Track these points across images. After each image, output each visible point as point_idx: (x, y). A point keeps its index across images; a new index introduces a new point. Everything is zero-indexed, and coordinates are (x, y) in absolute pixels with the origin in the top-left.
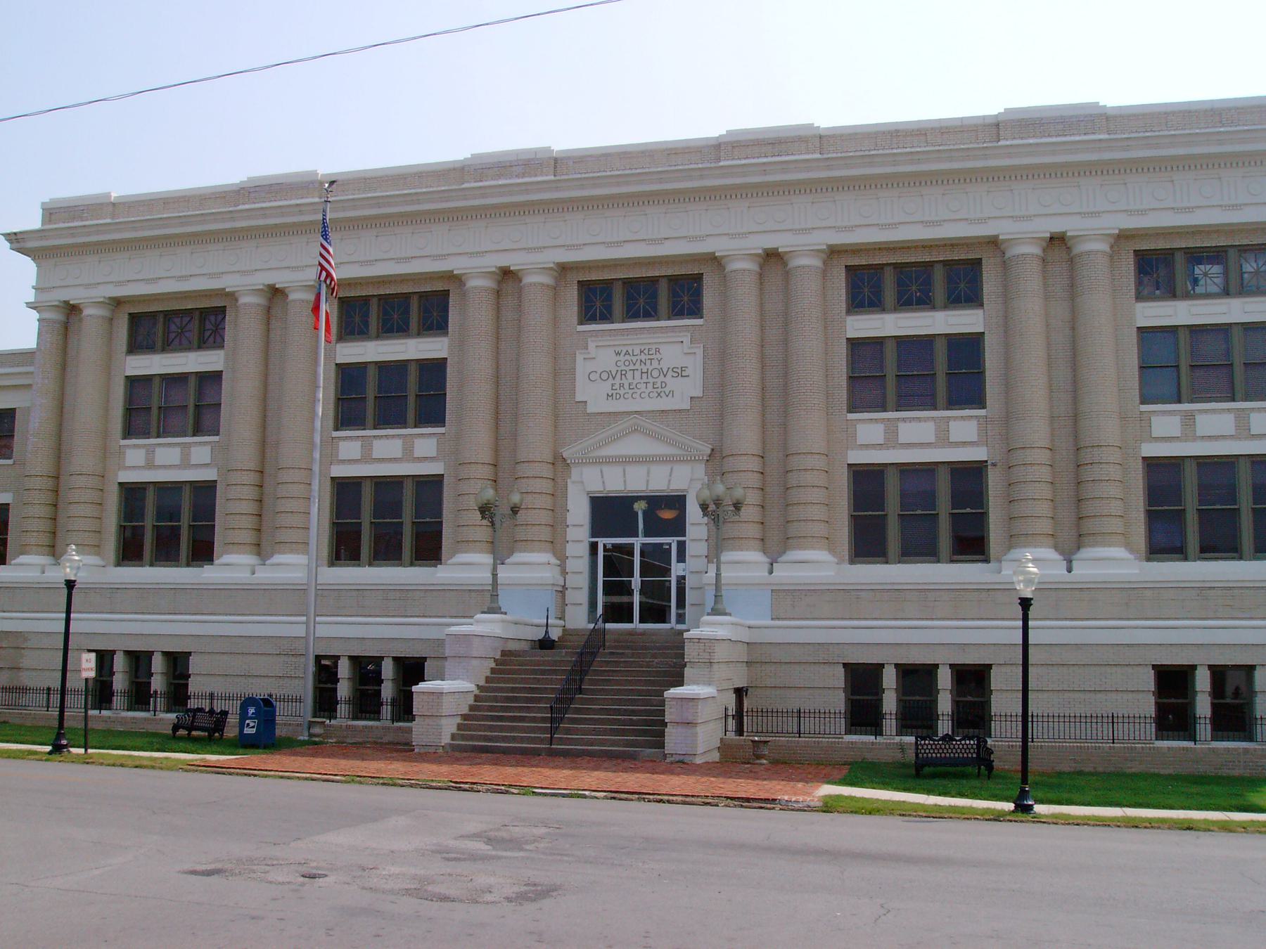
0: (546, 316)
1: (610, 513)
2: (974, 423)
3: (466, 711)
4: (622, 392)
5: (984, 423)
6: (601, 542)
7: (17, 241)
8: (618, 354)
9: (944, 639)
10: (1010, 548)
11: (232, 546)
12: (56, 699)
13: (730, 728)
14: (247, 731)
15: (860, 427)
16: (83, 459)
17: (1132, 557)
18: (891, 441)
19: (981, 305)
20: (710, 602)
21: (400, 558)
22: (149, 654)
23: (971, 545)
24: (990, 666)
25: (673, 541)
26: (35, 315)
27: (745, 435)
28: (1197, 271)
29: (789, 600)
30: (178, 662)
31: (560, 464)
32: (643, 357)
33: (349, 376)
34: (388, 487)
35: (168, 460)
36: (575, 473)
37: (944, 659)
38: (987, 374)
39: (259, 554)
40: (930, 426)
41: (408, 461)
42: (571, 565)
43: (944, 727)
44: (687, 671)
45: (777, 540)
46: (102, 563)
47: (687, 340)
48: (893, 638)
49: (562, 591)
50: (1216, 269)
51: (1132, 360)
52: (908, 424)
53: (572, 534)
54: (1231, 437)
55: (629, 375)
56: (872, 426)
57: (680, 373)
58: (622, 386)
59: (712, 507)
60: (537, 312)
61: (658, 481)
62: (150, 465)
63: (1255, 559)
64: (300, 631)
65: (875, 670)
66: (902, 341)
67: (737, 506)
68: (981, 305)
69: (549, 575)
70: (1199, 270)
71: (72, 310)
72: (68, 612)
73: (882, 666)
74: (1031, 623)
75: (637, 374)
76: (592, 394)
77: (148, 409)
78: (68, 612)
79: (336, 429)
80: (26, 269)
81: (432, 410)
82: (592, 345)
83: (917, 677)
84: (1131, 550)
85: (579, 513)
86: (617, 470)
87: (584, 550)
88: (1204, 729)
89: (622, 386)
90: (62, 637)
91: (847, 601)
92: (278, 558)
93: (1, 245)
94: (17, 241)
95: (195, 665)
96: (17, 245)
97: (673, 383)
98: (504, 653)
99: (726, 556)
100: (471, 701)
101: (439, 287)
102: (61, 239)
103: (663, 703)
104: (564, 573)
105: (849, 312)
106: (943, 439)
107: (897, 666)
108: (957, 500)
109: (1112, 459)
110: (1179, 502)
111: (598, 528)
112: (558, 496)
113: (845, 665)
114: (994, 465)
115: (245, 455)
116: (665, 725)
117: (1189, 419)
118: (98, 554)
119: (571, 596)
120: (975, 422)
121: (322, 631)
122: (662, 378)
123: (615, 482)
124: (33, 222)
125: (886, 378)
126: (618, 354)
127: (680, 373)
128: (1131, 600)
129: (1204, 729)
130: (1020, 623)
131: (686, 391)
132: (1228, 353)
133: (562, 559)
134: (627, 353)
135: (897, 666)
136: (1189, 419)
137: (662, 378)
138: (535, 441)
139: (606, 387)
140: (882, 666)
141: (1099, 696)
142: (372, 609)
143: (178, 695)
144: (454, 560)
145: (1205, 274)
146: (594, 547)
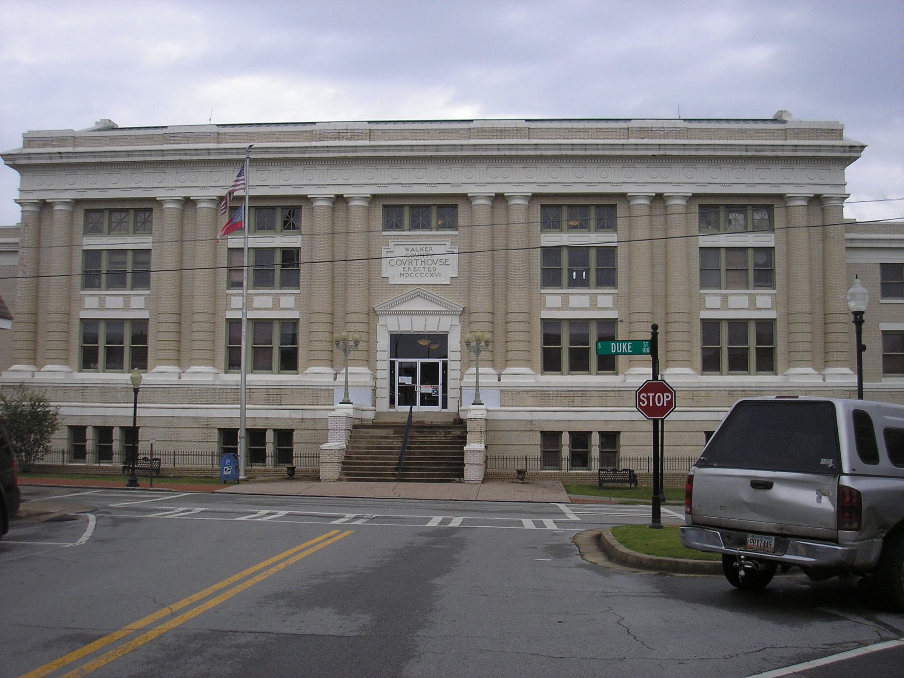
1: (401, 343)
2: (611, 297)
4: (409, 272)
5: (147, 298)
6: (398, 361)
7: (11, 160)
8: (407, 250)
10: (789, 367)
11: (312, 362)
13: (215, 462)
14: (225, 473)
15: (548, 297)
16: (54, 302)
17: (692, 372)
18: (565, 306)
19: (616, 231)
23: (290, 362)
24: (619, 432)
25: (440, 361)
26: (19, 208)
27: (481, 301)
28: (731, 217)
29: (509, 395)
30: (285, 436)
31: (372, 313)
33: (551, 254)
34: (738, 326)
35: (272, 304)
36: (381, 320)
37: (595, 428)
38: (619, 270)
39: (35, 364)
40: (587, 298)
42: (379, 374)
45: (501, 362)
46: (71, 370)
47: (448, 244)
48: (564, 417)
49: (374, 390)
50: (741, 216)
52: (574, 297)
53: (380, 356)
54: (123, 309)
55: (414, 262)
58: (409, 269)
59: (473, 344)
60: (357, 220)
61: (432, 325)
62: (102, 308)
63: (756, 374)
64: (237, 414)
65: (557, 435)
66: (571, 248)
67: (357, 343)
68: (616, 231)
69: (368, 380)
70: (732, 216)
71: (44, 205)
73: (113, 427)
75: (419, 262)
76: (392, 272)
77: (96, 271)
79: (228, 289)
80: (14, 176)
81: (142, 278)
82: (391, 244)
83: (580, 439)
84: (694, 369)
85: (384, 343)
86: (408, 318)
87: (386, 365)
88: (565, 464)
89: (409, 269)
90: (132, 419)
91: (543, 396)
92: (48, 367)
93: (864, 143)
94: (11, 160)
96: (11, 163)
97: (440, 269)
98: (355, 427)
100: (344, 454)
101: (295, 203)
102: (35, 160)
103: (463, 454)
104: (375, 378)
105: (542, 231)
106: (752, 306)
107: (570, 432)
108: (134, 340)
110: (747, 343)
112: (371, 334)
114: (622, 321)
115: (168, 303)
116: (464, 465)
117: (725, 298)
118: (67, 364)
119: (379, 392)
120: (611, 297)
121: (249, 414)
122: (433, 265)
123: (406, 325)
124: (15, 145)
125: (556, 269)
126: (407, 250)
129: (565, 464)
130: (133, 405)
131: (448, 272)
132: (746, 262)
133: (374, 370)
134: (413, 250)
135: (570, 432)
136: (725, 298)
137: (433, 265)
138: (356, 301)
139: (400, 269)
140: (86, 427)
141: (677, 448)
142: (262, 398)
143: (131, 453)
144: (155, 370)
145: (735, 219)
146: (392, 364)
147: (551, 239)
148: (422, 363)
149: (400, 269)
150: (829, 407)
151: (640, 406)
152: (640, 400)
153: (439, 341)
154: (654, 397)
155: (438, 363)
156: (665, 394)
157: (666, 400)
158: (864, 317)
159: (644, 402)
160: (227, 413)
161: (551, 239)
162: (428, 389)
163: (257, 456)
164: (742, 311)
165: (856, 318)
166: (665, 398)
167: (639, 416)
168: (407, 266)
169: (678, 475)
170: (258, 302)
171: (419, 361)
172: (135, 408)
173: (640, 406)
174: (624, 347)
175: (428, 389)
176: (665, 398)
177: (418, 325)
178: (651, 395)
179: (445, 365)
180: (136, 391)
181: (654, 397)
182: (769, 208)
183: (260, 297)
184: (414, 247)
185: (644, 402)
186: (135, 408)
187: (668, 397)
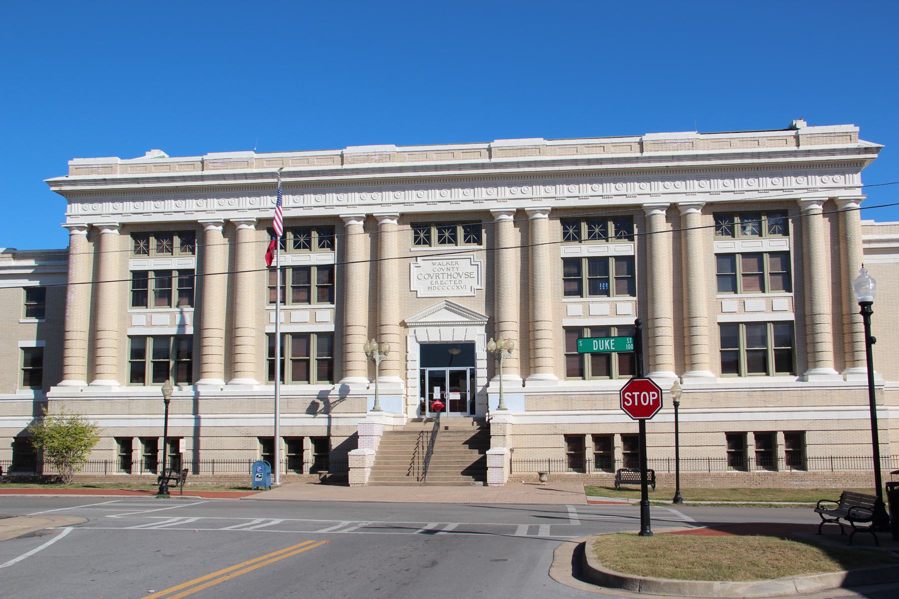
0: (397, 239)
1: (432, 353)
3: (372, 465)
9: (778, 419)
12: (673, 464)
14: (257, 480)
20: (371, 405)
21: (143, 381)
22: (744, 434)
25: (468, 369)
32: (448, 266)
41: (312, 323)
43: (619, 465)
44: (492, 440)
48: (752, 420)
51: (713, 271)
56: (576, 305)
57: (469, 275)
62: (150, 325)
72: (166, 414)
74: (169, 416)
78: (166, 414)
95: (809, 438)
99: (379, 379)
107: (621, 434)
109: (511, 328)
111: (424, 362)
113: (726, 433)
123: (435, 336)
126: (434, 264)
127: (469, 275)
128: (252, 401)
139: (428, 283)
140: (132, 438)
147: (574, 250)
148: (452, 373)
149: (428, 283)
150: (294, 379)
151: (624, 405)
152: (625, 400)
153: (466, 351)
154: (639, 396)
155: (465, 372)
156: (651, 393)
157: (652, 398)
158: (873, 307)
159: (628, 402)
160: (263, 424)
161: (574, 250)
162: (456, 396)
163: (295, 463)
164: (758, 314)
165: (863, 308)
166: (651, 397)
167: (627, 418)
168: (434, 279)
169: (698, 475)
170: (297, 316)
171: (448, 370)
172: (166, 419)
173: (624, 405)
174: (607, 344)
175: (456, 396)
176: (651, 397)
177: (447, 335)
178: (636, 394)
179: (473, 375)
180: (167, 402)
181: (639, 396)
182: (785, 213)
183: (301, 312)
184: (441, 261)
185: (628, 402)
186: (166, 419)
187: (654, 395)
